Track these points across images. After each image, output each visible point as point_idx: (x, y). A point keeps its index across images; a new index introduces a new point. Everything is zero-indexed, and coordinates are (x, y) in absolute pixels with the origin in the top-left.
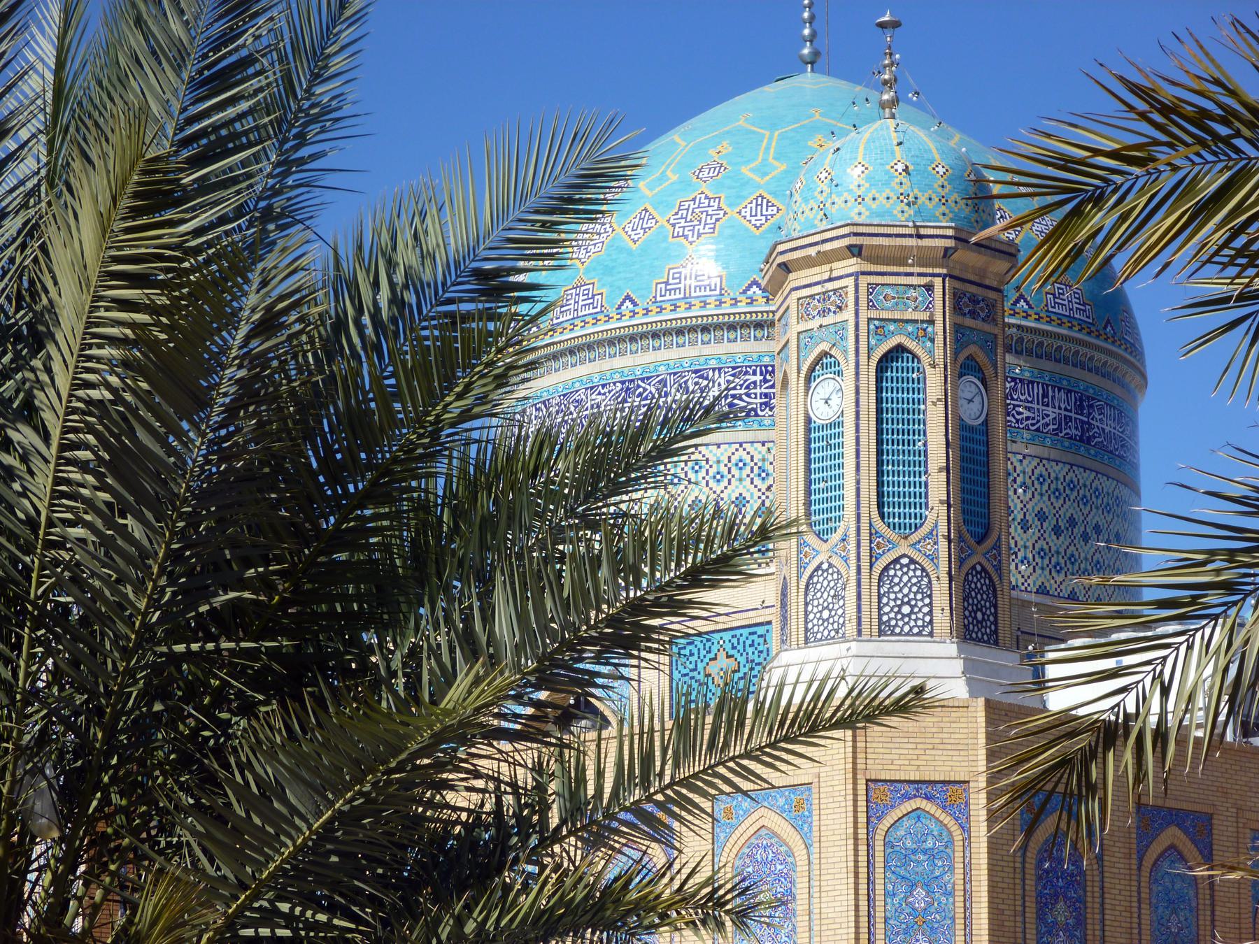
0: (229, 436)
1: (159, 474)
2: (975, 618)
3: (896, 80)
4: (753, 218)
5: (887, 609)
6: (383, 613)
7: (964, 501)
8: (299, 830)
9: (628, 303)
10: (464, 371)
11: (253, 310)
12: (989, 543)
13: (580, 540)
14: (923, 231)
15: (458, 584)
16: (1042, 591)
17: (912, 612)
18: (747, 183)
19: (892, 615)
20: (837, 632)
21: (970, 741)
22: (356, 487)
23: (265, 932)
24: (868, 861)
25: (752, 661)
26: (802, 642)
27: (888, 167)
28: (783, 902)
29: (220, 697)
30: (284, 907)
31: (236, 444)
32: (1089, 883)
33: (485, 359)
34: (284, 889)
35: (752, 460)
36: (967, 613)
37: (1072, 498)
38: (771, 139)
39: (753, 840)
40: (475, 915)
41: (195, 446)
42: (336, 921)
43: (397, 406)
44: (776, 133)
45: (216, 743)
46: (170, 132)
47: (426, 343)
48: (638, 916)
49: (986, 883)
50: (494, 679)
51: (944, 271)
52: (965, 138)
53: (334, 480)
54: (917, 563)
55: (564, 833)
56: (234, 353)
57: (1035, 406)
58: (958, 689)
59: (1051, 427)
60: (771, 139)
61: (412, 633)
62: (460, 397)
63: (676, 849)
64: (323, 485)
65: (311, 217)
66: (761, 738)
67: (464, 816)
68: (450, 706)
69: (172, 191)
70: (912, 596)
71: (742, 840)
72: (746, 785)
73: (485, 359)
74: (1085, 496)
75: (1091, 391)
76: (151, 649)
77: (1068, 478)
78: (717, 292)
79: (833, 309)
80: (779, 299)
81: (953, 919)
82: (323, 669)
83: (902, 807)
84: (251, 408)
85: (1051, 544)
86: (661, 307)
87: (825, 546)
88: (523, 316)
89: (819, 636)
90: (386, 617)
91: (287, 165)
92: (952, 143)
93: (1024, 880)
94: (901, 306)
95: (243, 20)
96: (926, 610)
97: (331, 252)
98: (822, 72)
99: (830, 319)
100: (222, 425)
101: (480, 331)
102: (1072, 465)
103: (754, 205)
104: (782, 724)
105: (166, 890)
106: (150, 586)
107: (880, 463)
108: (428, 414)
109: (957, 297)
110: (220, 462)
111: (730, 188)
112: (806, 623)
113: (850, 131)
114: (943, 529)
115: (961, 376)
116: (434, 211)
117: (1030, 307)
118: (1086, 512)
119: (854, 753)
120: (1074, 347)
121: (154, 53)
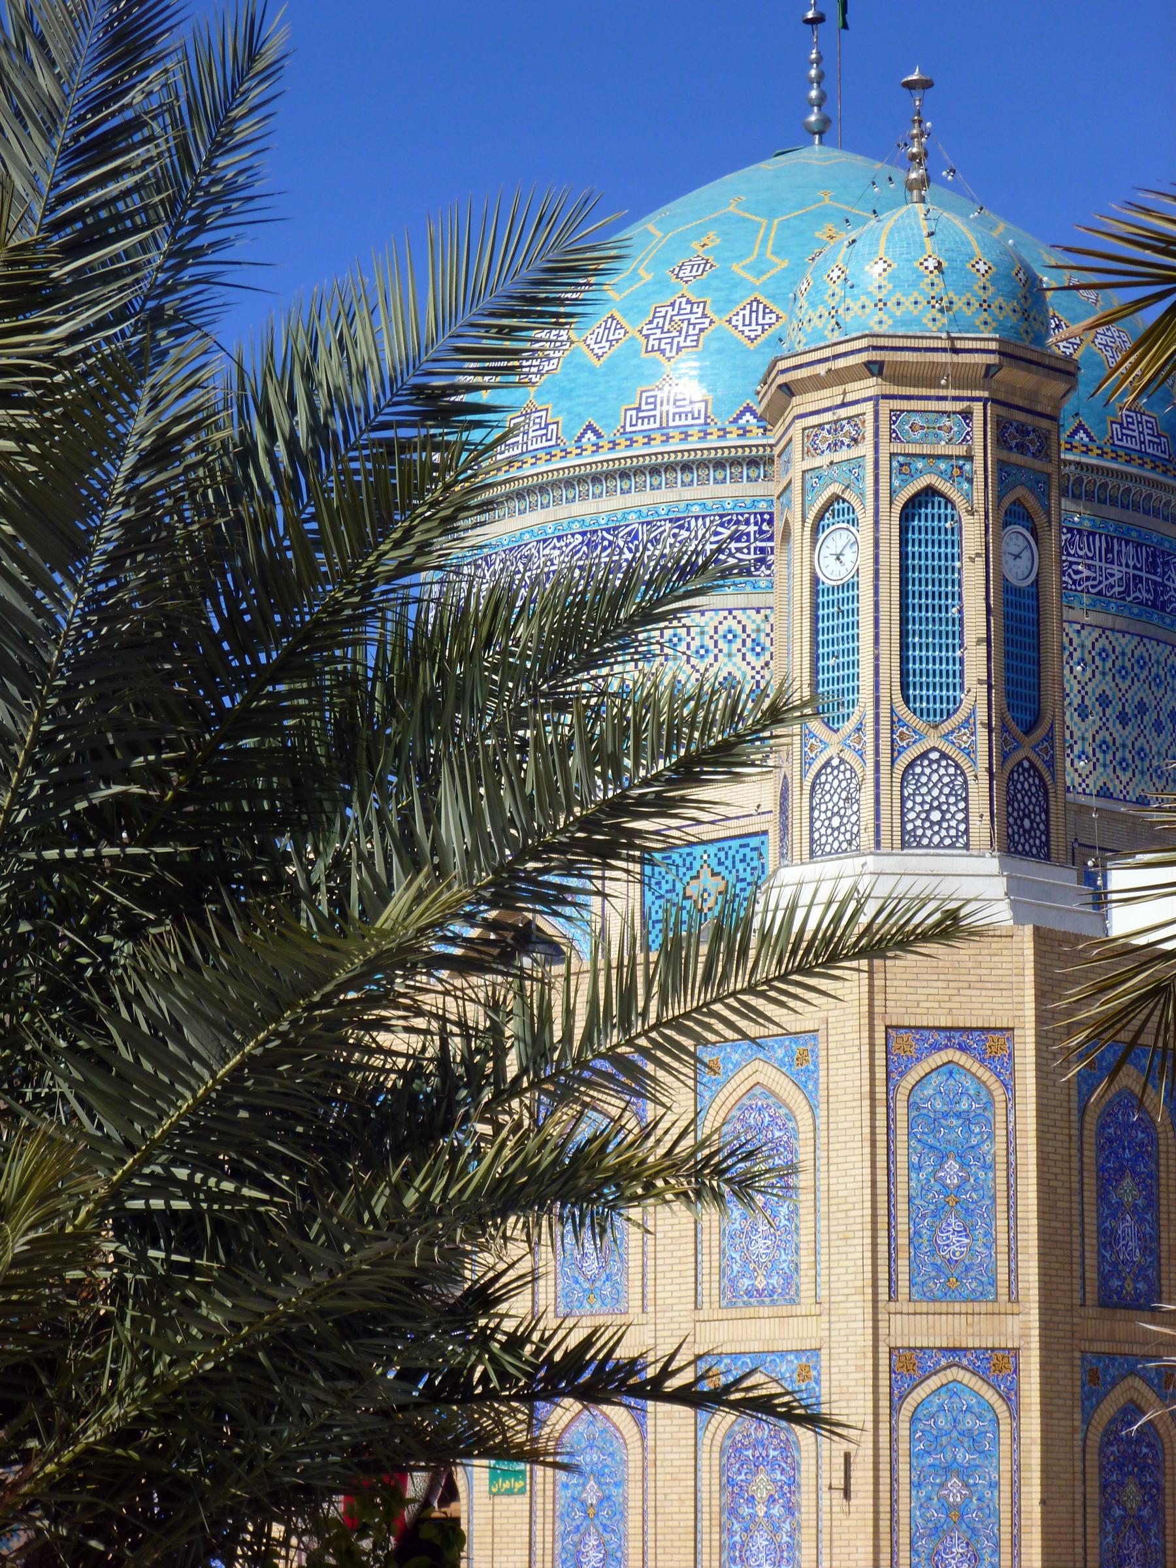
0: (112, 592)
1: (26, 640)
2: (1022, 826)
3: (926, 154)
4: (746, 329)
5: (912, 815)
6: (301, 813)
7: (1008, 681)
8: (200, 1078)
9: (590, 434)
10: (403, 513)
11: (142, 435)
12: (1040, 732)
13: (546, 724)
14: (959, 344)
15: (393, 779)
16: (1104, 793)
17: (943, 819)
18: (739, 283)
19: (918, 823)
20: (850, 844)
21: (1015, 979)
22: (269, 657)
23: (157, 1204)
24: (888, 1127)
25: (744, 880)
26: (806, 856)
27: (917, 264)
28: (793, 1169)
29: (100, 919)
30: (182, 1173)
31: (120, 601)
32: (1162, 1155)
33: (428, 497)
34: (181, 1150)
35: (744, 631)
36: (1011, 820)
37: (1142, 677)
38: (769, 229)
39: (745, 1101)
40: (417, 1183)
41: (70, 604)
42: (246, 1192)
43: (320, 556)
44: (776, 222)
45: (95, 972)
46: (38, 214)
47: (356, 478)
48: (618, 1186)
49: (1035, 1154)
50: (440, 893)
51: (986, 394)
52: (1013, 228)
53: (240, 650)
54: (950, 758)
55: (525, 1084)
56: (118, 488)
57: (1097, 563)
58: (1001, 913)
59: (1116, 589)
60: (769, 229)
61: (338, 838)
62: (398, 545)
63: (663, 1105)
64: (227, 654)
65: (213, 322)
66: (764, 972)
67: (401, 1062)
68: (388, 926)
69: (42, 287)
70: (943, 799)
71: (732, 1100)
72: (752, 1029)
73: (428, 497)
74: (1158, 676)
75: (1167, 544)
76: (15, 855)
77: (1137, 653)
78: (702, 421)
79: (846, 441)
80: (779, 429)
81: (994, 1198)
82: (228, 880)
83: (930, 1060)
84: (140, 558)
85: (1115, 735)
86: (631, 439)
87: (835, 738)
88: (476, 445)
89: (828, 849)
90: (305, 817)
91: (181, 256)
92: (995, 234)
93: (1081, 1150)
94: (931, 438)
95: (130, 73)
96: (960, 816)
97: (235, 367)
98: (833, 145)
99: (843, 454)
100: (103, 579)
101: (423, 464)
102: (1142, 637)
103: (747, 312)
104: (794, 953)
105: (36, 1152)
106: (15, 777)
107: (904, 634)
108: (358, 566)
109: (1002, 427)
110: (102, 622)
111: (718, 289)
112: (812, 832)
113: (869, 219)
114: (982, 715)
115: (1006, 525)
116: (365, 314)
117: (1091, 439)
118: (1159, 695)
119: (871, 992)
120: (1146, 490)
121: (18, 114)
